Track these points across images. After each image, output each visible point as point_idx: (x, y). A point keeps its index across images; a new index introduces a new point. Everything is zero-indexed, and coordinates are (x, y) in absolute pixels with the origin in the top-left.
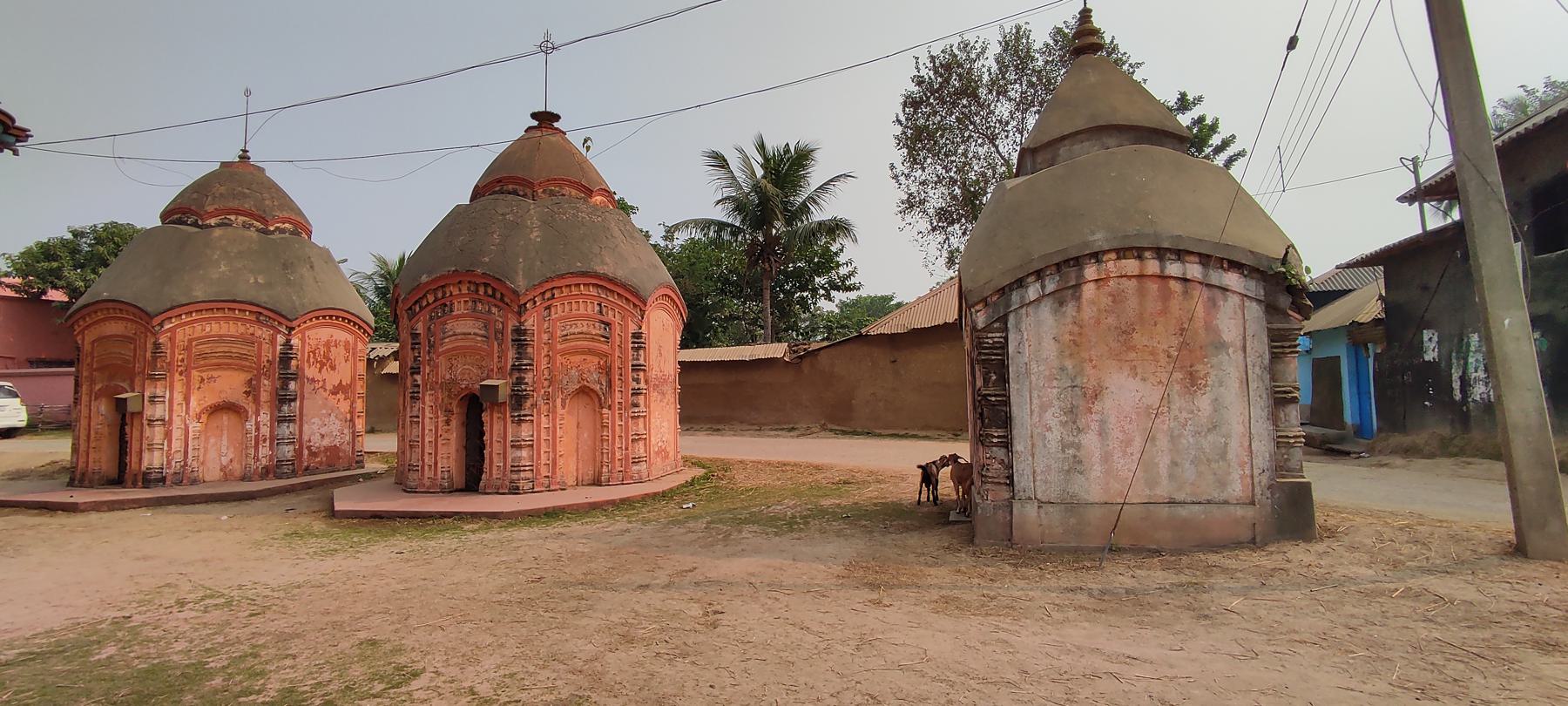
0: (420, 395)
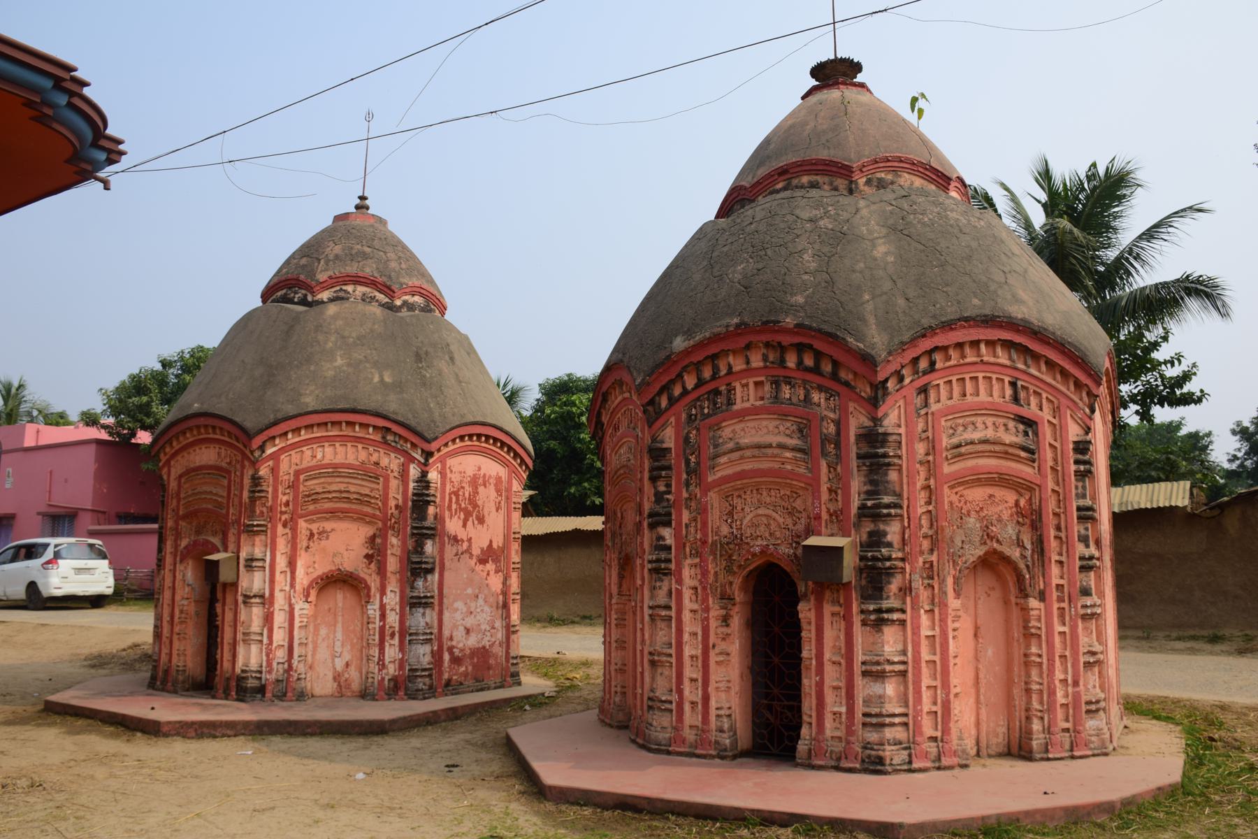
0: (673, 566)
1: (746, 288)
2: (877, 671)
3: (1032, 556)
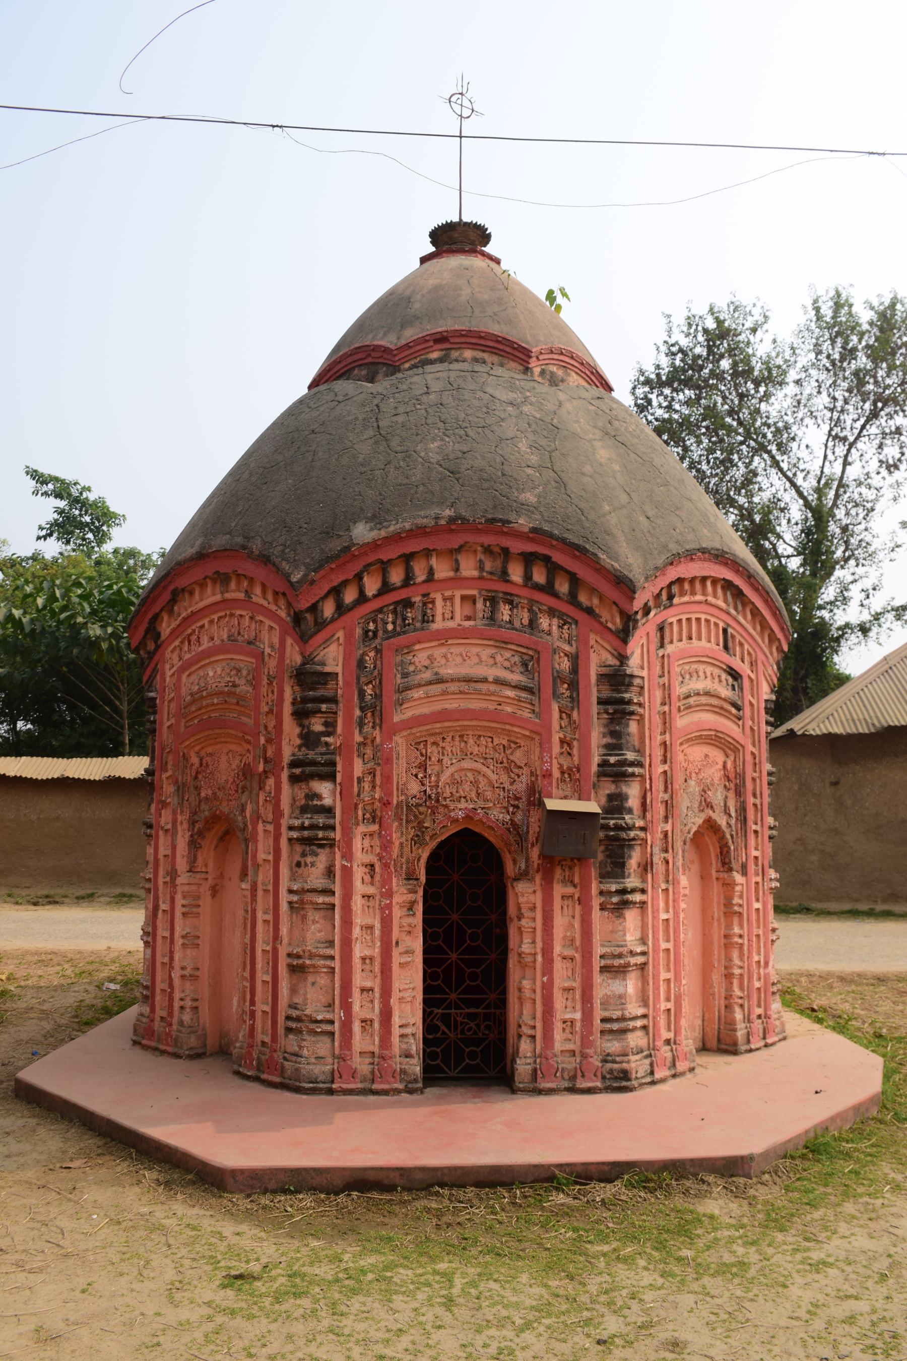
0: (338, 835)
2: (620, 966)
3: (736, 824)
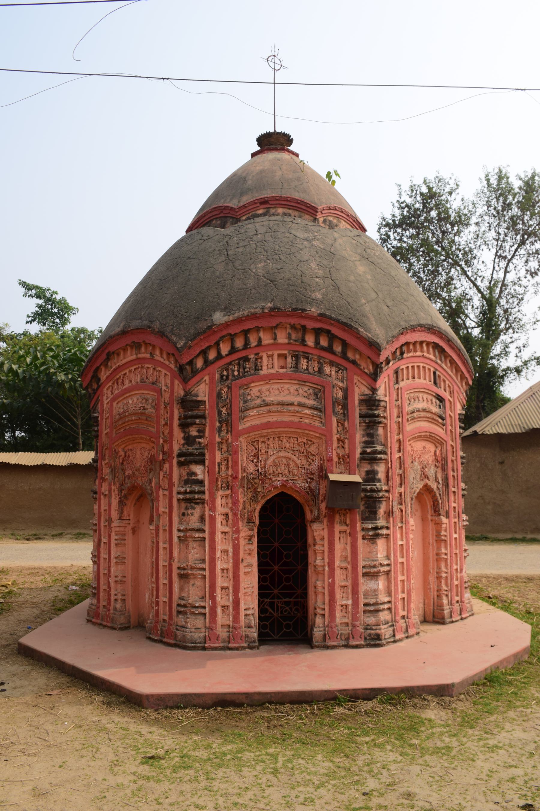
0: (207, 497)
1: (272, 281)
2: (374, 573)
3: (442, 488)
